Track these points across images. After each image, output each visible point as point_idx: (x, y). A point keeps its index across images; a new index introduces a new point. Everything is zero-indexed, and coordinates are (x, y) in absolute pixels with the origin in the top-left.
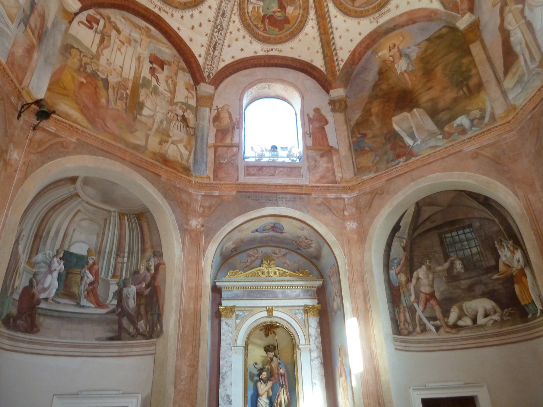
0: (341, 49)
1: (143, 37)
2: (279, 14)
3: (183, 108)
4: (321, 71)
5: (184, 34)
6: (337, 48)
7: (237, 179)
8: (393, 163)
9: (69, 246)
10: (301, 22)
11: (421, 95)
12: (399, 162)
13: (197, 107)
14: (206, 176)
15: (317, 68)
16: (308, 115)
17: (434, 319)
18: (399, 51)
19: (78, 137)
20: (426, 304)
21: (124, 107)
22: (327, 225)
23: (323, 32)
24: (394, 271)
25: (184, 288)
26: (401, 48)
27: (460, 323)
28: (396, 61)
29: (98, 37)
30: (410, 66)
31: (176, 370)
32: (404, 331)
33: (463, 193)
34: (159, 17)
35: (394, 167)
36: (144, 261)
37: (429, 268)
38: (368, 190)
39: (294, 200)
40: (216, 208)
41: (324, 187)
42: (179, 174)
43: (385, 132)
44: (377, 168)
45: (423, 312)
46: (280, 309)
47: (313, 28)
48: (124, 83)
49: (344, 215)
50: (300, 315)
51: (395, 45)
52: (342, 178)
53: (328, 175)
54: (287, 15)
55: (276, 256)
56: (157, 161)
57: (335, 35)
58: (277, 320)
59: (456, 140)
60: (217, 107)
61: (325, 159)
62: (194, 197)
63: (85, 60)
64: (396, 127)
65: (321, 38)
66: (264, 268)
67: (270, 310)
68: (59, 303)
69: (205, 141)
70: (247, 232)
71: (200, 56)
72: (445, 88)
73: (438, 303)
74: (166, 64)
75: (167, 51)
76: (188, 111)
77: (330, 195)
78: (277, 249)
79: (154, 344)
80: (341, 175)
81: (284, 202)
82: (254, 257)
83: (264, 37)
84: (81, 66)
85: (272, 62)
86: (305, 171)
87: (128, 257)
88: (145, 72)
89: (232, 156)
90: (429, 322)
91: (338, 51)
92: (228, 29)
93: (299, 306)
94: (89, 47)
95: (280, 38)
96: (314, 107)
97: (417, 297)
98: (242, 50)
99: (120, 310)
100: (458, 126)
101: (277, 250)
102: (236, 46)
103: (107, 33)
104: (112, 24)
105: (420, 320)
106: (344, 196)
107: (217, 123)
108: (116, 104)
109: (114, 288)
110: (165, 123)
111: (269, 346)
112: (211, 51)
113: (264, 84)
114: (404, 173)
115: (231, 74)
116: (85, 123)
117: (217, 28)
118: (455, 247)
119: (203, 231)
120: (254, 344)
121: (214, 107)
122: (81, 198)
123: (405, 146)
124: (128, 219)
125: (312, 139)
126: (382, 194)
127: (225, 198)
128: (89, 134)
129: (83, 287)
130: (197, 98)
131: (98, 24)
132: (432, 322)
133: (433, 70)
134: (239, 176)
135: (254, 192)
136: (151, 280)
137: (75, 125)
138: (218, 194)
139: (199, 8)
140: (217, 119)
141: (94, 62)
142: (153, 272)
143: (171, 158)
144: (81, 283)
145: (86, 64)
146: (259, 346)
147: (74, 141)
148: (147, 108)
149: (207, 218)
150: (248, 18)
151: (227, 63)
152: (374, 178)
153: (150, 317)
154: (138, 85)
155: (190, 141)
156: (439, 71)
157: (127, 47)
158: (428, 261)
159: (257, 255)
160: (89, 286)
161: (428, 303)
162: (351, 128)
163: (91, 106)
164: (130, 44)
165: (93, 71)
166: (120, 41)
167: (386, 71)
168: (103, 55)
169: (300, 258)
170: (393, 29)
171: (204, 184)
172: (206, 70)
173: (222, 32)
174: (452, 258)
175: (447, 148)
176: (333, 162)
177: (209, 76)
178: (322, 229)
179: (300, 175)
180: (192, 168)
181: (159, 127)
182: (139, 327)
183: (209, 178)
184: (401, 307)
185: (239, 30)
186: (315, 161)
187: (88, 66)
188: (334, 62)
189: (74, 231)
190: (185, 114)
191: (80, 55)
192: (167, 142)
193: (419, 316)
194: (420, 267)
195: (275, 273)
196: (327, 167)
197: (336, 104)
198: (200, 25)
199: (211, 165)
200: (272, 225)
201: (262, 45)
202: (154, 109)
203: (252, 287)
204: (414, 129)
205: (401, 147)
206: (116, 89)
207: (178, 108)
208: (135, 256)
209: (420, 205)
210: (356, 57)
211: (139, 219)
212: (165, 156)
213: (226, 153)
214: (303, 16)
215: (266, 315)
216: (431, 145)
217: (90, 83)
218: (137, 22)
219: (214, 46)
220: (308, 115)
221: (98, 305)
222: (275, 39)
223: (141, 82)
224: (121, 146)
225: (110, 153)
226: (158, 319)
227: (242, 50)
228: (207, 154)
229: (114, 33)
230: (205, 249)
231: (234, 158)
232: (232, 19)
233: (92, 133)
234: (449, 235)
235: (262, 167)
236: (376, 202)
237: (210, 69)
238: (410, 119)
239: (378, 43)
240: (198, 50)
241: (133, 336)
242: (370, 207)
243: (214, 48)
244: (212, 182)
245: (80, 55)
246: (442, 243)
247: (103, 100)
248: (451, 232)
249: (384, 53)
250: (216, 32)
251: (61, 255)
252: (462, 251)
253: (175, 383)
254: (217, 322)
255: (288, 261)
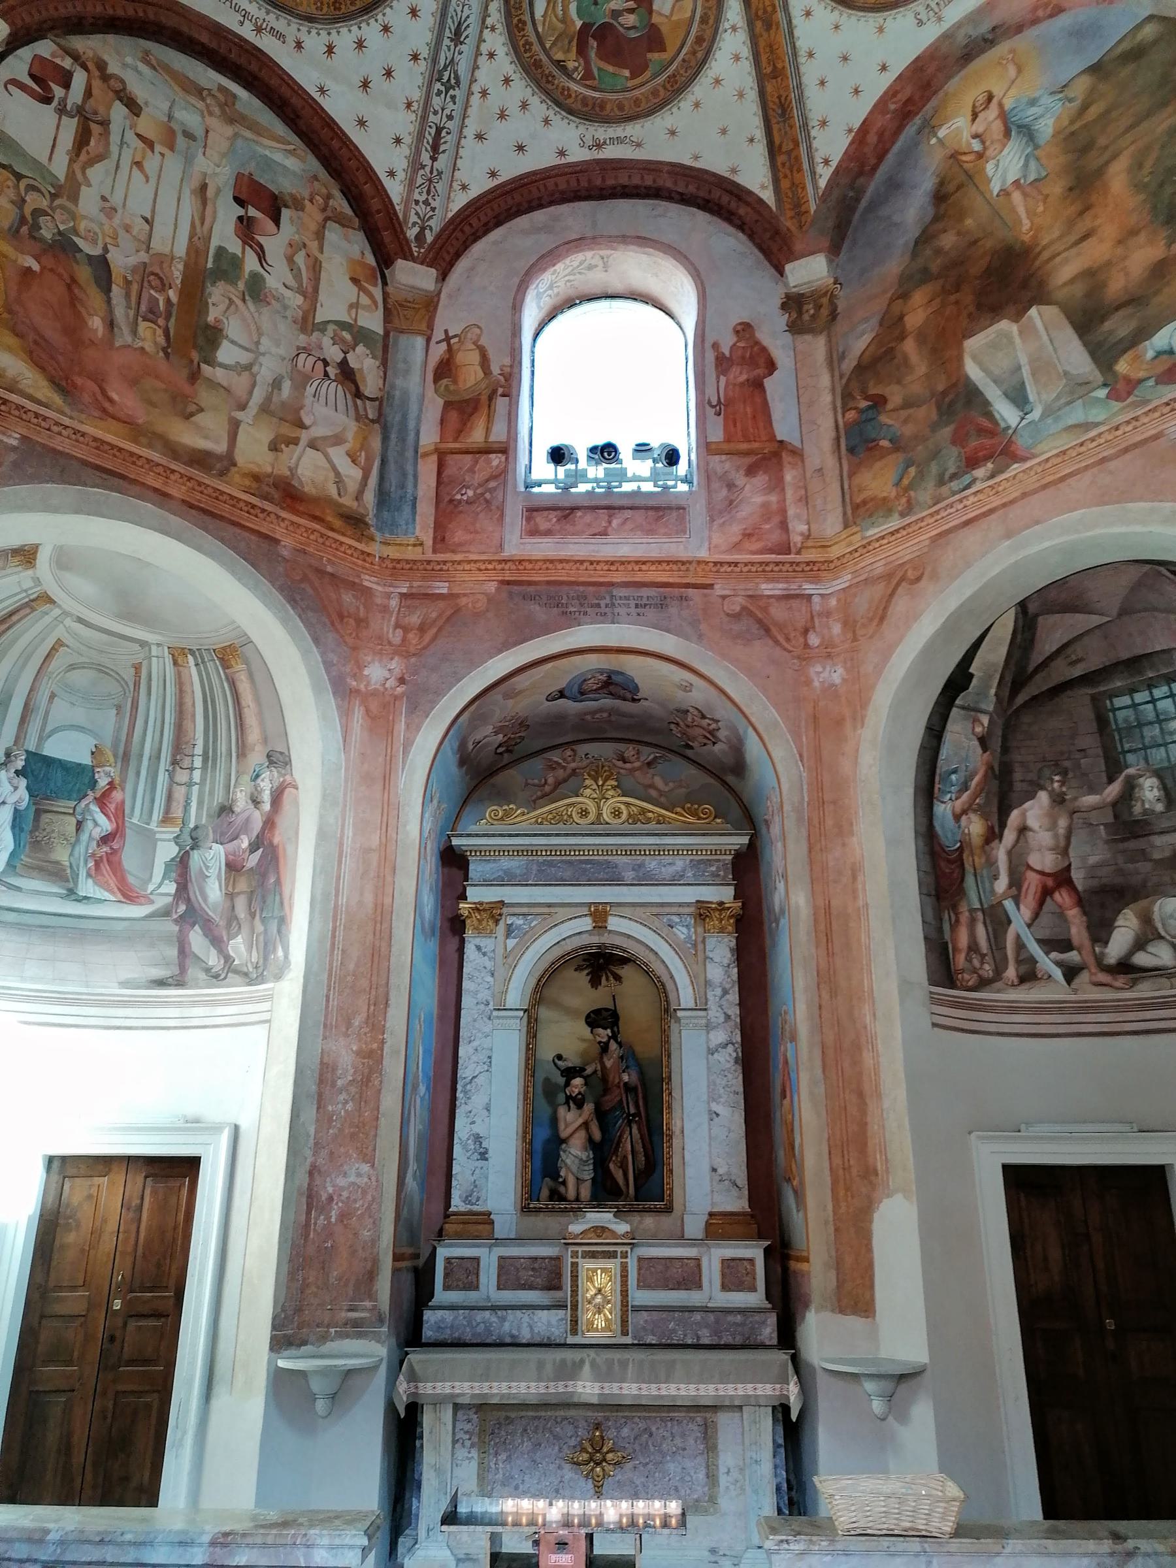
0: (824, 123)
1: (214, 123)
2: (630, 19)
3: (343, 340)
4: (761, 201)
5: (341, 106)
6: (811, 124)
7: (501, 546)
8: (955, 485)
9: (41, 739)
10: (699, 40)
11: (1058, 259)
12: (974, 480)
13: (387, 334)
14: (412, 541)
15: (750, 193)
16: (715, 346)
17: (1066, 945)
18: (1003, 115)
19: (25, 432)
20: (1041, 903)
21: (161, 340)
22: (750, 672)
23: (769, 70)
24: (949, 806)
25: (347, 849)
26: (1008, 104)
27: (1141, 959)
28: (989, 153)
29: (70, 126)
30: (1033, 165)
31: (322, 1063)
32: (966, 976)
33: (1162, 569)
34: (257, 53)
35: (957, 497)
36: (246, 778)
37: (1059, 800)
38: (879, 568)
39: (662, 605)
40: (440, 629)
41: (753, 564)
42: (331, 534)
43: (940, 387)
44: (908, 501)
45: (1029, 926)
46: (627, 912)
47: (737, 58)
48: (158, 271)
49: (806, 645)
50: (685, 930)
51: (990, 98)
52: (807, 537)
53: (767, 526)
54: (655, 19)
55: (628, 766)
56: (266, 497)
57: (805, 80)
58: (618, 941)
59: (1147, 402)
60: (446, 331)
61: (761, 479)
62: (379, 601)
63: (34, 201)
64: (973, 371)
65: (762, 94)
66: (586, 800)
67: (599, 914)
68: (18, 889)
69: (411, 437)
70: (532, 699)
71: (392, 174)
72: (1134, 232)
73: (1080, 902)
74: (286, 206)
75: (288, 164)
76: (360, 349)
77: (768, 588)
78: (631, 747)
79: (269, 998)
80: (804, 528)
81: (633, 610)
82: (564, 768)
83: (585, 101)
84: (23, 220)
85: (610, 182)
86: (698, 515)
87: (204, 768)
88: (224, 234)
89: (487, 481)
90: (1047, 954)
91: (813, 133)
92: (473, 80)
93: (680, 905)
94: (44, 159)
95: (637, 102)
96: (735, 320)
97: (1016, 882)
98: (521, 148)
99: (182, 908)
100: (1159, 354)
101: (630, 751)
102: (503, 134)
103: (96, 113)
104: (112, 82)
105: (1020, 946)
106: (808, 588)
107: (445, 382)
108: (134, 332)
109: (167, 851)
110: (287, 386)
111: (597, 1012)
112: (425, 157)
113: (589, 254)
114: (985, 515)
115: (487, 229)
116: (43, 389)
117: (439, 80)
118: (1142, 737)
119: (403, 694)
120: (557, 1005)
121: (438, 334)
122: (59, 607)
123: (992, 428)
124: (197, 665)
125: (725, 419)
126: (918, 579)
127: (463, 601)
128: (57, 424)
129: (83, 850)
130: (385, 308)
131: (67, 86)
132: (1054, 955)
133: (1100, 172)
134: (507, 537)
135: (548, 583)
136: (263, 829)
137: (14, 398)
138: (445, 591)
139: (380, 17)
140: (445, 370)
141: (62, 207)
142: (267, 807)
143: (308, 489)
144: (78, 840)
145: (38, 213)
146: (570, 1012)
147: (15, 443)
148: (233, 342)
149: (413, 660)
150: (533, 38)
151: (474, 192)
152: (897, 531)
153: (259, 927)
154: (204, 271)
155: (365, 438)
156: (1118, 178)
157: (162, 155)
158: (1057, 778)
159: (573, 765)
160: (98, 846)
161: (1048, 899)
162: (844, 381)
163: (55, 336)
164: (172, 148)
165: (60, 233)
166: (138, 135)
167: (960, 187)
168: (89, 185)
169: (693, 771)
170: (988, 42)
171: (408, 562)
172: (413, 218)
173: (457, 92)
174: (1131, 771)
175: (1117, 428)
176: (783, 489)
177: (420, 237)
178: (739, 687)
179: (682, 528)
180: (370, 519)
181: (268, 399)
182: (232, 954)
183: (421, 544)
184: (964, 908)
185: (507, 81)
186: (731, 486)
187: (42, 220)
188: (800, 170)
189: (53, 696)
190: (351, 357)
191: (17, 187)
192: (295, 441)
193: (1018, 937)
194: (1031, 796)
195: (617, 813)
196: (765, 505)
197: (806, 307)
198: (389, 73)
199: (426, 510)
200: (603, 678)
201: (582, 129)
202: (253, 344)
203: (552, 850)
204: (1026, 372)
205: (981, 431)
206: (135, 287)
207: (326, 341)
208: (222, 764)
209: (1032, 608)
210: (873, 147)
211: (226, 665)
212: (289, 485)
213: (472, 470)
214: (704, 20)
215: (590, 928)
216: (1070, 422)
217: (51, 270)
218: (191, 75)
219: (433, 140)
220: (715, 346)
221: (124, 895)
222: (621, 107)
223: (210, 265)
224: (156, 456)
225: (123, 477)
226: (279, 931)
227: (521, 148)
228: (415, 476)
229: (118, 112)
230: (408, 745)
231: (492, 484)
232: (484, 48)
233: (66, 421)
234: (1125, 700)
235: (574, 509)
236: (900, 605)
237: (425, 214)
238: (1018, 340)
239: (941, 94)
240: (385, 156)
241: (216, 976)
242: (882, 619)
243: (435, 148)
244: (429, 555)
245: (17, 187)
246: (1102, 722)
247: (96, 323)
248: (1132, 691)
249: (957, 129)
250: (439, 93)
251: (20, 764)
252: (1162, 749)
253: (320, 1095)
254: (454, 943)
255: (658, 781)
